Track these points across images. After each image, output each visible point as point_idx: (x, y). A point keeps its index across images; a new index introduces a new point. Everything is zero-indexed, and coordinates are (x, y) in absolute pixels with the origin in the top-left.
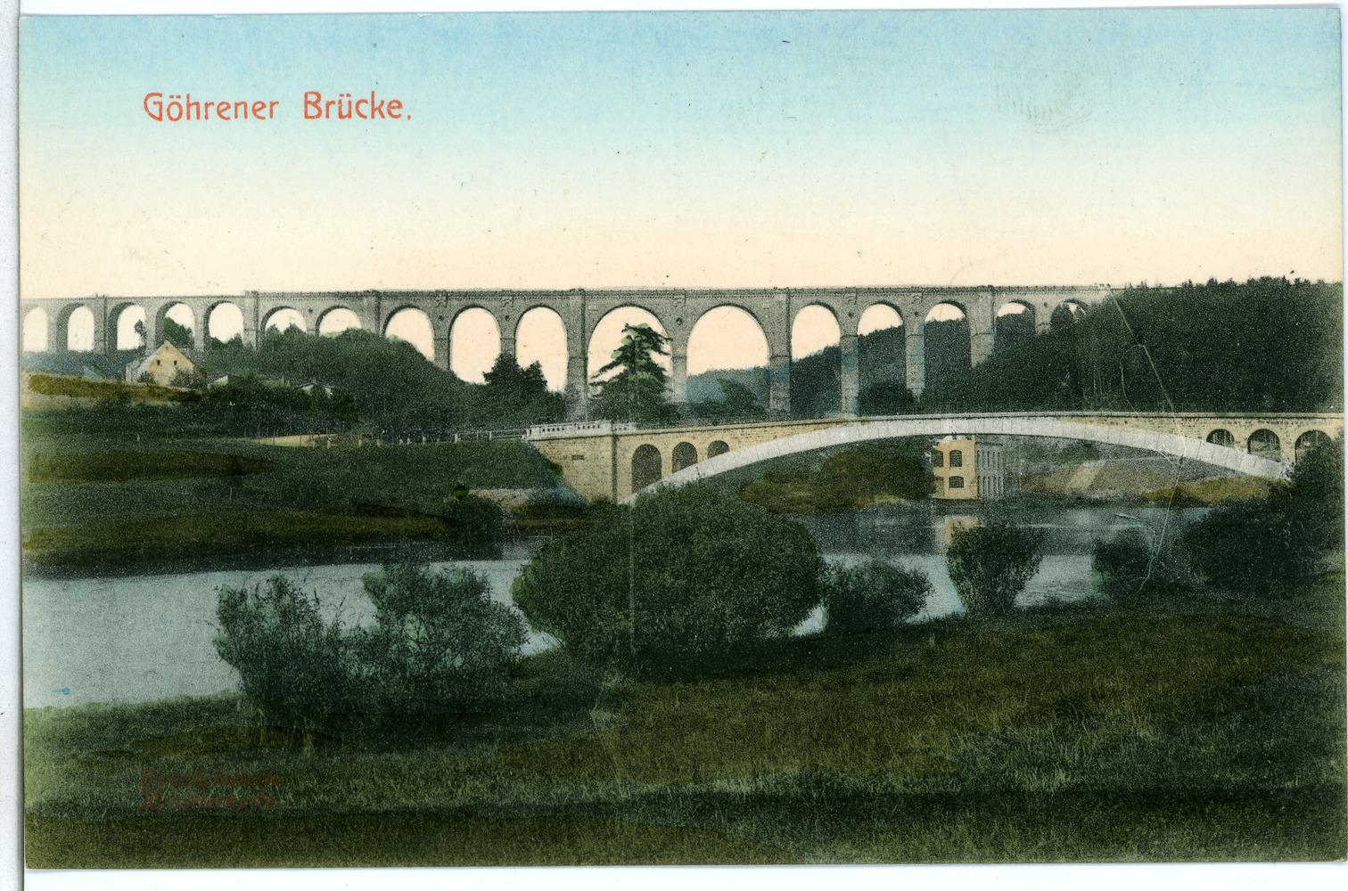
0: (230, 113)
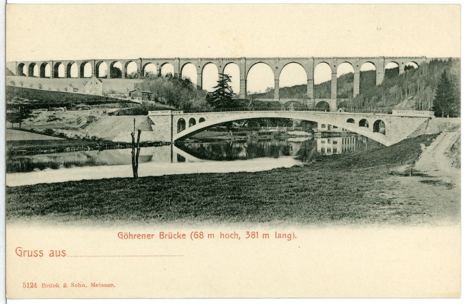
0: (141, 237)
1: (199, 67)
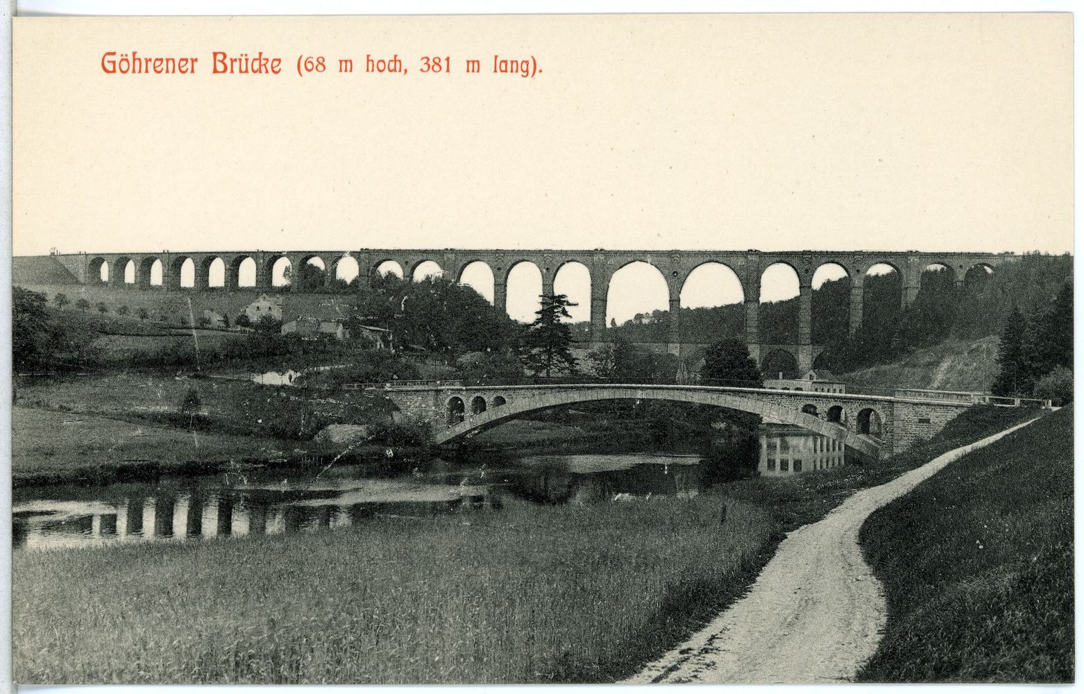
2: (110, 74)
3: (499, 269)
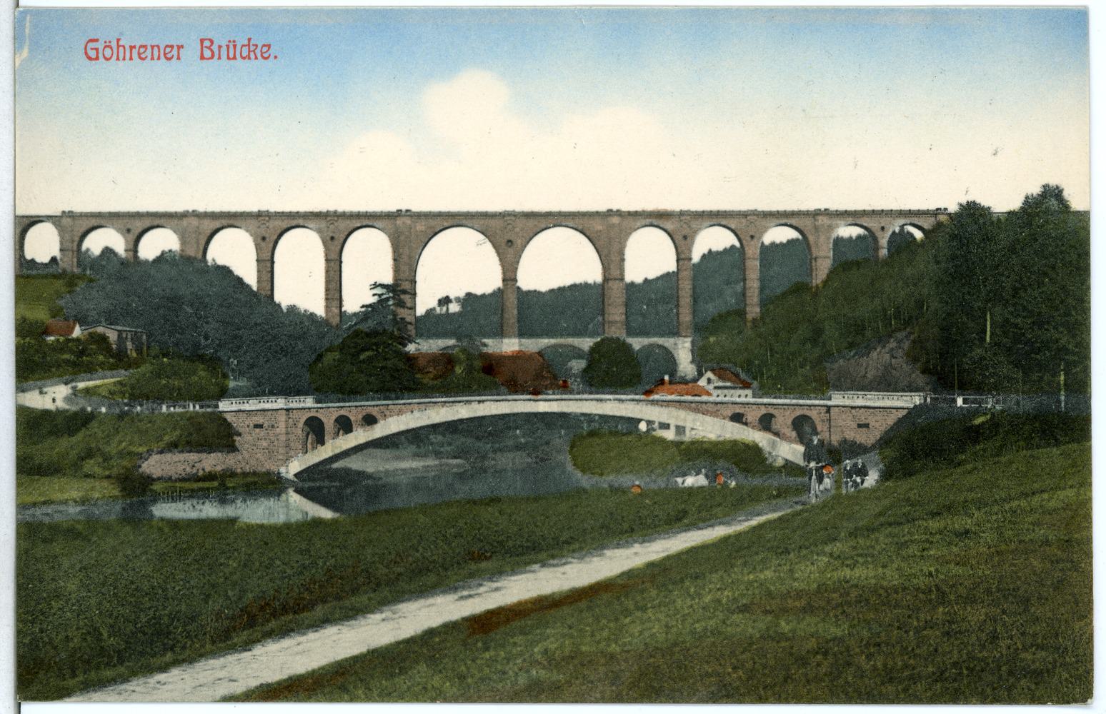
1: (264, 239)
2: (94, 62)
3: (264, 239)
